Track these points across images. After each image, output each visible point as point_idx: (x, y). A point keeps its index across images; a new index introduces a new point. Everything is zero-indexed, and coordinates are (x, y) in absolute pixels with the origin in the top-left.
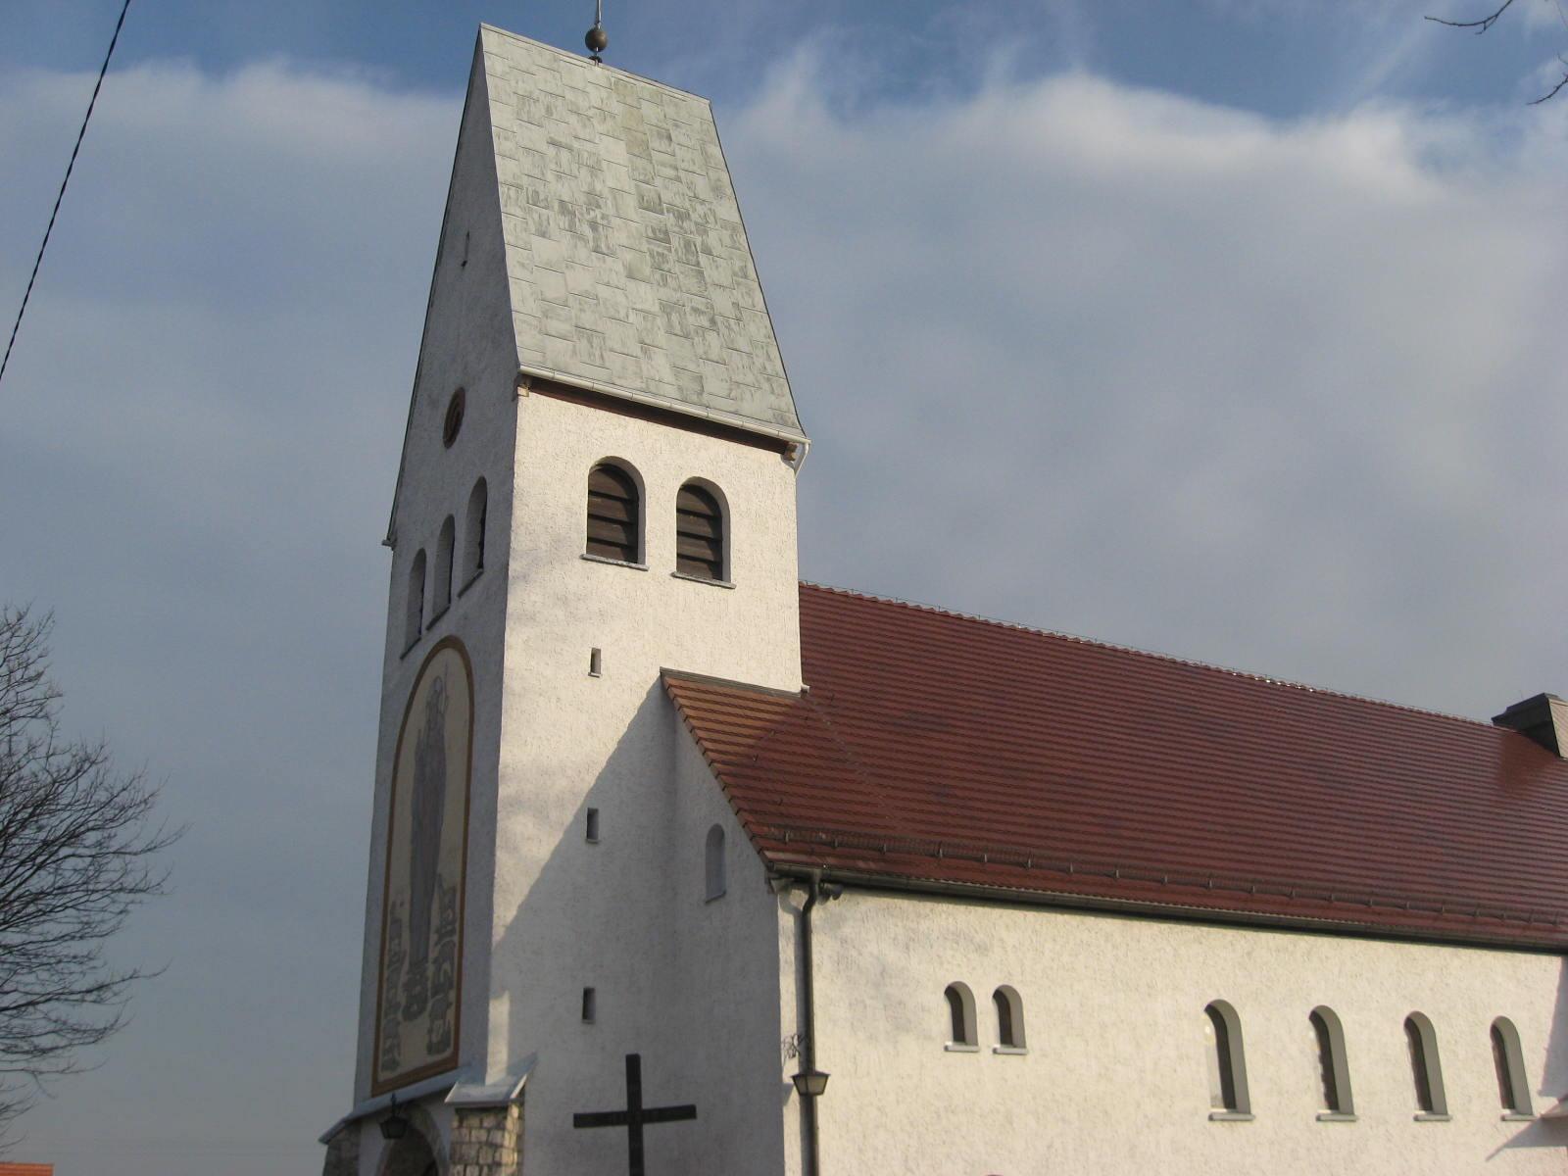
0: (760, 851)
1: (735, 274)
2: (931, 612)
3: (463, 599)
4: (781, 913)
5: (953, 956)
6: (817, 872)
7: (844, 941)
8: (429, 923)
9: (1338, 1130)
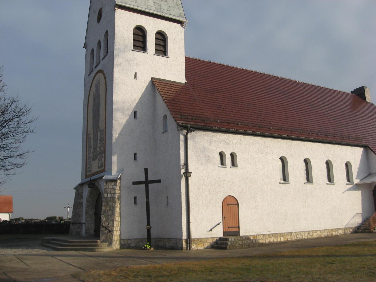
0: (176, 121)
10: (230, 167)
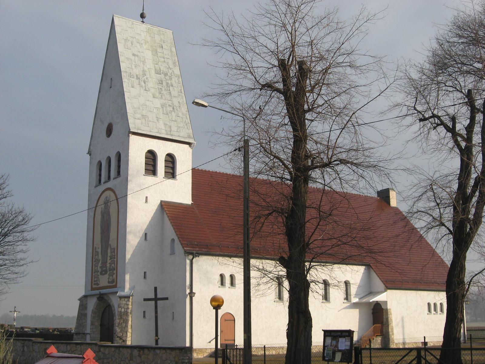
0: (183, 247)
1: (179, 92)
3: (115, 180)
8: (107, 254)
10: (229, 288)
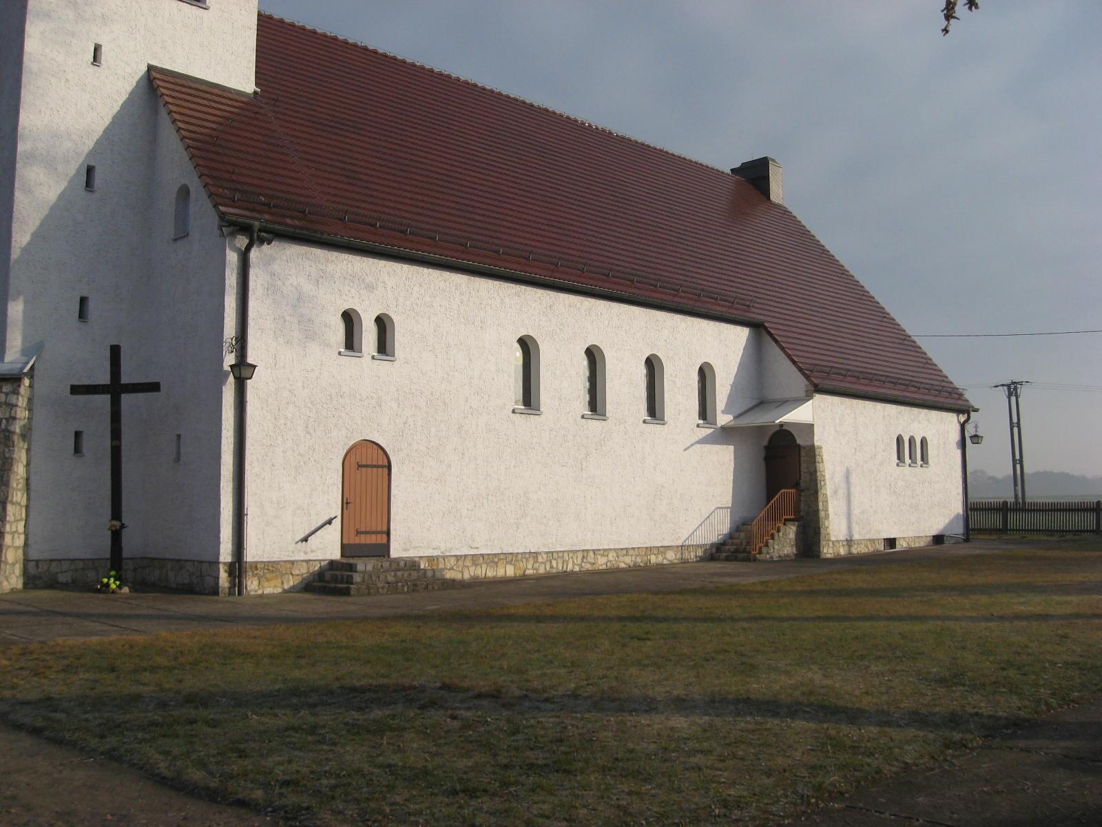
2: (355, 46)
4: (228, 250)
5: (349, 291)
6: (257, 224)
7: (273, 274)
9: (595, 425)
